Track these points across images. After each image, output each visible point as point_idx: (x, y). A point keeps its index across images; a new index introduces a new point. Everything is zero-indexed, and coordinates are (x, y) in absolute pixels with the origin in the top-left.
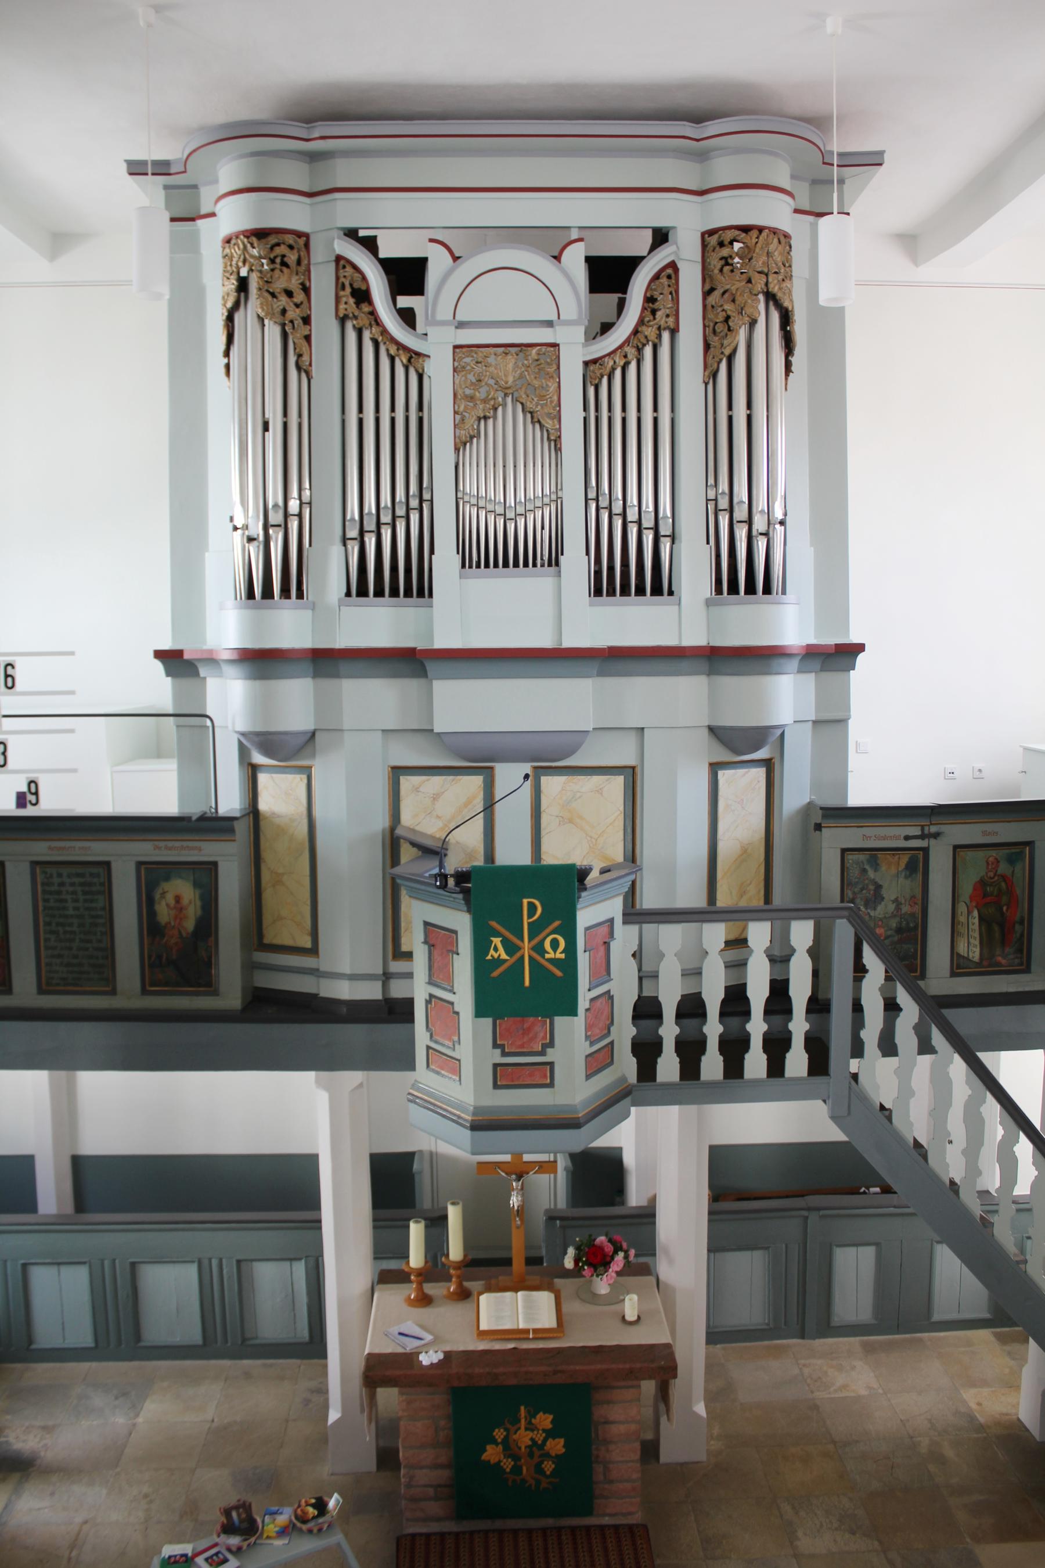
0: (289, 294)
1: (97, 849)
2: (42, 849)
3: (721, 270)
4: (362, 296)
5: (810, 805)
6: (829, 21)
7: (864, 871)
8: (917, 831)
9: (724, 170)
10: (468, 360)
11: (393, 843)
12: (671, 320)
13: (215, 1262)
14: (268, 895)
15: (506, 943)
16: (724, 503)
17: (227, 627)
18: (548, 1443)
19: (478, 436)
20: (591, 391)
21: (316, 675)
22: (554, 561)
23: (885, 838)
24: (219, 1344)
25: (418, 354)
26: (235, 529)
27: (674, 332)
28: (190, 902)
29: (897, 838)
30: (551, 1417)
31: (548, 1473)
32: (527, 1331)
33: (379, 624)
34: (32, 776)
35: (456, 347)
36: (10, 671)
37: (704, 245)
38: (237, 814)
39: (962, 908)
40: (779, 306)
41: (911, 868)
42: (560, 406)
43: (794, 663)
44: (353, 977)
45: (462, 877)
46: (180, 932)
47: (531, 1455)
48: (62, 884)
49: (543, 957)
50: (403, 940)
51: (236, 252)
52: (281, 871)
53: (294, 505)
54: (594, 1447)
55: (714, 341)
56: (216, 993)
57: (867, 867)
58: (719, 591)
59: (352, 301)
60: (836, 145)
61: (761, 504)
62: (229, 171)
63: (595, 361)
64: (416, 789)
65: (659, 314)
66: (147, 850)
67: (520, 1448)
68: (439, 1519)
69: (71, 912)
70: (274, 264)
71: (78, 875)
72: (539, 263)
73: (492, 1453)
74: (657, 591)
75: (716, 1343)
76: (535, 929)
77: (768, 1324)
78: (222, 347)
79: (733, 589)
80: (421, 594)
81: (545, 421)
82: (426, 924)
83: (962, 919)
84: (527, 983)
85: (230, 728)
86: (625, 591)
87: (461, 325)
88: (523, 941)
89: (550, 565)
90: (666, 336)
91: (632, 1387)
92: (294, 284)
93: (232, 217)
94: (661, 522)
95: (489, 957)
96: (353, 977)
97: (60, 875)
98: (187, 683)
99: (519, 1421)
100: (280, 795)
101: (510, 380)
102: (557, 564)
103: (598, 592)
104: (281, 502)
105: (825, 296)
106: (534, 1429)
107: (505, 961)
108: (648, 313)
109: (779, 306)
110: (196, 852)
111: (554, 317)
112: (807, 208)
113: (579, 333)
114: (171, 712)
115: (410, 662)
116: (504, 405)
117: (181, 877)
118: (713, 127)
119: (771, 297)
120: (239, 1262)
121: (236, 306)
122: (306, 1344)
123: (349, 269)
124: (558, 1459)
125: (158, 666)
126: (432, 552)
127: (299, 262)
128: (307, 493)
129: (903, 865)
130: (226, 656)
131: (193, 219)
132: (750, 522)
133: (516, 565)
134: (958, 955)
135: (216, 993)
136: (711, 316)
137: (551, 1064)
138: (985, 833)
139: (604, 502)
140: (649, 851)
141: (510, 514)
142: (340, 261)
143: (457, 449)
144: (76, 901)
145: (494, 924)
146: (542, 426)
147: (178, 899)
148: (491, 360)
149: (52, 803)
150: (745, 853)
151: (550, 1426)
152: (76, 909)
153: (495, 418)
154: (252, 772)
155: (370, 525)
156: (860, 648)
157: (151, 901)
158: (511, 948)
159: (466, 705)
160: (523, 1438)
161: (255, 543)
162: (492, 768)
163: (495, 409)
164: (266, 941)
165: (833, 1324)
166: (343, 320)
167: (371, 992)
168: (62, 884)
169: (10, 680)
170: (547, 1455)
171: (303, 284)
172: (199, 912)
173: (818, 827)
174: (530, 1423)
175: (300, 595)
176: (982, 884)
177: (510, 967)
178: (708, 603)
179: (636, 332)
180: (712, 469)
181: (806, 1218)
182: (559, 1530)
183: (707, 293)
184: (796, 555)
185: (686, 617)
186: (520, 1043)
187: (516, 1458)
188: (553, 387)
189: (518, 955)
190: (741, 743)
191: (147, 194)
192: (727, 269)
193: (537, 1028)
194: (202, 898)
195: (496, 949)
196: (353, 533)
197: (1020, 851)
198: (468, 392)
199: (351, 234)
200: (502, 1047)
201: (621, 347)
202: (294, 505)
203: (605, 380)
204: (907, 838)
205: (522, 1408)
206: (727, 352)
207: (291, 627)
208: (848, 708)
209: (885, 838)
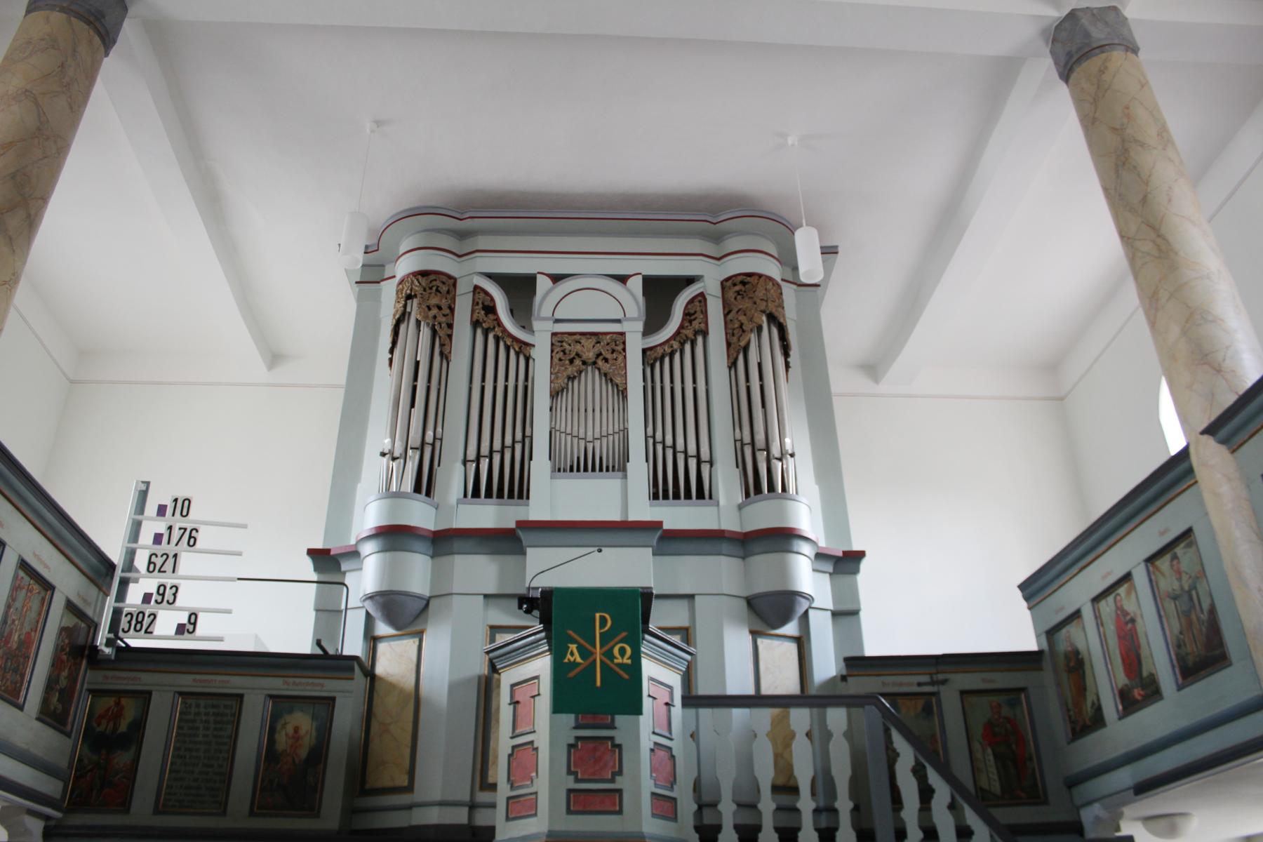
0: (440, 308)
2: (187, 681)
4: (490, 309)
8: (926, 679)
15: (580, 648)
16: (747, 439)
23: (901, 684)
27: (705, 333)
33: (486, 515)
37: (723, 288)
39: (977, 746)
44: (442, 804)
50: (490, 773)
56: (317, 816)
69: (200, 739)
70: (431, 290)
71: (214, 706)
72: (614, 287)
74: (700, 495)
76: (605, 638)
78: (390, 346)
79: (758, 490)
80: (520, 497)
83: (979, 755)
84: (598, 684)
86: (676, 496)
87: (557, 321)
88: (595, 646)
93: (404, 267)
96: (442, 804)
100: (393, 660)
103: (656, 497)
107: (580, 664)
119: (772, 318)
123: (482, 295)
126: (531, 458)
127: (448, 292)
128: (439, 429)
129: (920, 708)
133: (593, 470)
134: (982, 789)
135: (317, 816)
137: (620, 791)
138: (984, 680)
141: (590, 438)
143: (552, 397)
144: (207, 729)
147: (296, 730)
152: (204, 736)
156: (860, 555)
157: (272, 730)
158: (585, 653)
159: (549, 568)
164: (368, 786)
168: (197, 714)
175: (428, 494)
176: (989, 726)
177: (585, 669)
179: (678, 333)
180: (737, 422)
185: (725, 509)
189: (591, 659)
195: (572, 654)
200: (575, 774)
204: (919, 684)
207: (420, 515)
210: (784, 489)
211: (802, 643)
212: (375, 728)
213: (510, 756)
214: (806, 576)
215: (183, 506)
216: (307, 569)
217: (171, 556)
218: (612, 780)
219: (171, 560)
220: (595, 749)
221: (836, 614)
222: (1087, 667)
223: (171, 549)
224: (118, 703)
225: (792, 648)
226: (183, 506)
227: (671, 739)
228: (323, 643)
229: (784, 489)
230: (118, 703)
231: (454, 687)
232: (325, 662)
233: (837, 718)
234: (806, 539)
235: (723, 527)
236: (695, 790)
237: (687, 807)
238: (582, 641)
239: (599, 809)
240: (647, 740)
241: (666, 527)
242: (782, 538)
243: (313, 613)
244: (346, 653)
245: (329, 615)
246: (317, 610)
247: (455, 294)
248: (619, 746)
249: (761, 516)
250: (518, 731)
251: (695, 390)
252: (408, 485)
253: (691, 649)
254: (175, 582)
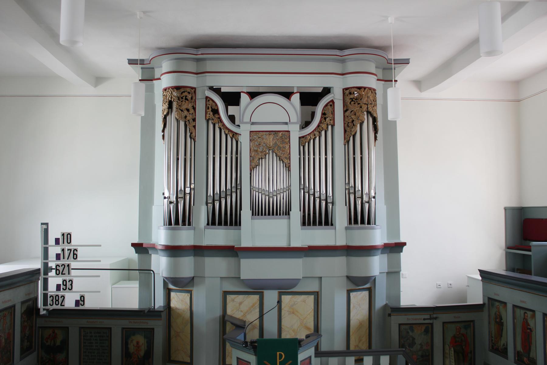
0: (188, 110)
1: (106, 323)
2: (84, 322)
3: (350, 103)
4: (216, 111)
5: (386, 305)
6: (389, 19)
7: (408, 332)
9: (351, 66)
10: (255, 137)
11: (224, 320)
12: (332, 122)
14: (173, 340)
16: (352, 191)
17: (160, 236)
19: (259, 165)
20: (302, 148)
21: (195, 255)
22: (287, 213)
23: (416, 319)
25: (236, 134)
26: (165, 198)
27: (333, 126)
33: (219, 236)
34: (82, 294)
35: (251, 132)
36: (75, 252)
37: (344, 94)
38: (162, 310)
39: (447, 347)
40: (372, 115)
41: (426, 331)
42: (290, 154)
43: (380, 251)
45: (252, 342)
48: (91, 336)
51: (168, 94)
53: (188, 190)
55: (348, 129)
57: (409, 331)
58: (350, 223)
59: (211, 113)
60: (393, 56)
61: (366, 190)
62: (166, 65)
63: (303, 137)
64: (233, 300)
65: (327, 119)
66: (126, 323)
70: (181, 99)
74: (327, 224)
78: (162, 129)
79: (356, 222)
80: (236, 225)
81: (285, 160)
82: (238, 358)
83: (447, 351)
85: (161, 275)
86: (314, 224)
87: (253, 124)
89: (286, 215)
90: (330, 127)
92: (190, 106)
93: (166, 81)
94: (328, 198)
97: (91, 333)
98: (144, 256)
100: (179, 301)
101: (270, 145)
102: (289, 214)
103: (304, 224)
104: (183, 189)
105: (390, 117)
108: (323, 119)
109: (372, 115)
111: (288, 121)
112: (382, 79)
113: (297, 127)
114: (137, 269)
115: (231, 251)
116: (269, 154)
118: (347, 52)
119: (369, 113)
121: (168, 114)
123: (211, 101)
125: (133, 249)
126: (241, 209)
127: (192, 98)
129: (423, 330)
130: (160, 247)
131: (152, 80)
132: (362, 198)
136: (346, 120)
139: (306, 190)
140: (324, 326)
142: (207, 99)
146: (283, 162)
147: (138, 343)
148: (264, 137)
149: (89, 304)
150: (361, 324)
153: (265, 158)
154: (168, 292)
155: (217, 197)
156: (404, 244)
157: (127, 344)
159: (253, 269)
161: (173, 204)
162: (263, 292)
163: (265, 155)
164: (172, 359)
166: (208, 121)
169: (75, 256)
171: (193, 106)
173: (390, 315)
175: (189, 224)
178: (347, 228)
179: (318, 126)
183: (345, 111)
184: (380, 209)
185: (337, 235)
188: (287, 147)
190: (359, 282)
191: (136, 73)
192: (352, 103)
196: (210, 201)
197: (469, 324)
198: (255, 149)
199: (211, 88)
201: (313, 132)
202: (188, 190)
203: (307, 144)
204: (424, 319)
206: (353, 134)
207: (186, 237)
208: (400, 268)
209: (416, 319)
215: (67, 237)
217: (66, 266)
219: (66, 268)
222: (504, 328)
223: (66, 262)
224: (54, 332)
226: (67, 237)
230: (54, 332)
247: (197, 93)
251: (326, 159)
254: (71, 278)
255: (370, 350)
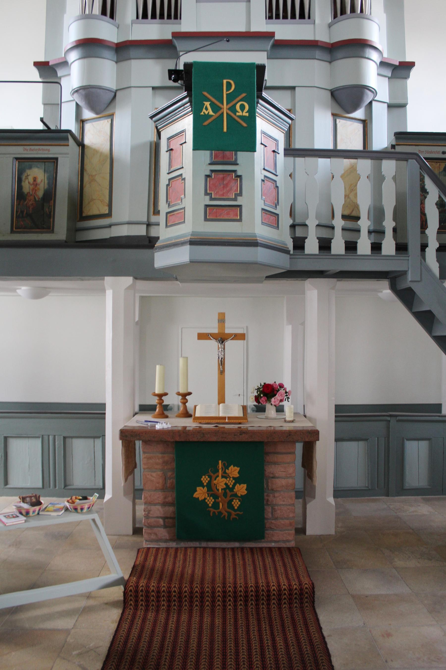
13: (51, 438)
15: (213, 105)
18: (236, 487)
23: (431, 152)
24: (51, 488)
28: (42, 181)
29: (438, 153)
30: (238, 469)
31: (236, 508)
32: (224, 418)
33: (153, 31)
44: (129, 223)
46: (35, 198)
47: (225, 495)
49: (235, 114)
52: (94, 174)
54: (265, 494)
56: (53, 232)
67: (218, 490)
68: (166, 541)
73: (200, 493)
74: (302, 16)
75: (338, 498)
76: (230, 98)
77: (368, 487)
79: (343, 12)
84: (225, 130)
88: (223, 104)
91: (290, 453)
95: (202, 113)
96: (129, 223)
99: (218, 471)
100: (95, 135)
106: (227, 477)
107: (212, 116)
110: (47, 152)
117: (38, 167)
120: (65, 438)
122: (101, 489)
124: (243, 498)
135: (53, 232)
137: (240, 206)
145: (205, 93)
147: (35, 179)
151: (238, 475)
156: (411, 65)
157: (20, 180)
158: (215, 108)
160: (220, 483)
165: (405, 488)
167: (141, 231)
170: (235, 495)
172: (46, 186)
174: (225, 472)
175: (112, 16)
181: (389, 421)
182: (242, 549)
185: (320, 26)
186: (221, 193)
187: (215, 496)
189: (220, 112)
193: (232, 184)
194: (49, 179)
195: (207, 109)
205: (220, 462)
207: (107, 31)
208: (407, 98)
209: (431, 152)
210: (362, 11)
211: (366, 124)
212: (86, 178)
213: (168, 185)
214: (372, 75)
216: (35, 74)
218: (235, 199)
220: (223, 179)
221: (390, 106)
225: (360, 126)
227: (277, 176)
228: (44, 120)
229: (362, 11)
231: (134, 149)
232: (51, 135)
233: (389, 167)
234: (375, 48)
235: (317, 39)
236: (291, 215)
237: (286, 221)
238: (213, 100)
239: (226, 217)
240: (259, 174)
241: (277, 37)
242: (358, 46)
243: (42, 106)
244: (63, 128)
245: (53, 105)
246: (44, 104)
248: (240, 177)
249: (345, 31)
250: (172, 169)
252: (97, 10)
253: (292, 116)
255: (364, 150)
